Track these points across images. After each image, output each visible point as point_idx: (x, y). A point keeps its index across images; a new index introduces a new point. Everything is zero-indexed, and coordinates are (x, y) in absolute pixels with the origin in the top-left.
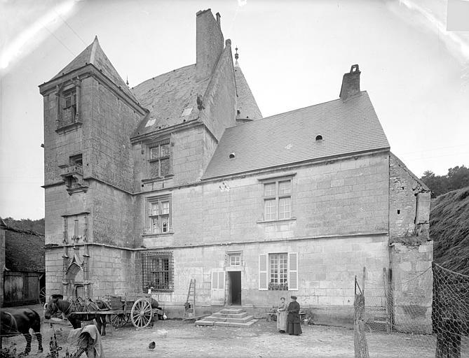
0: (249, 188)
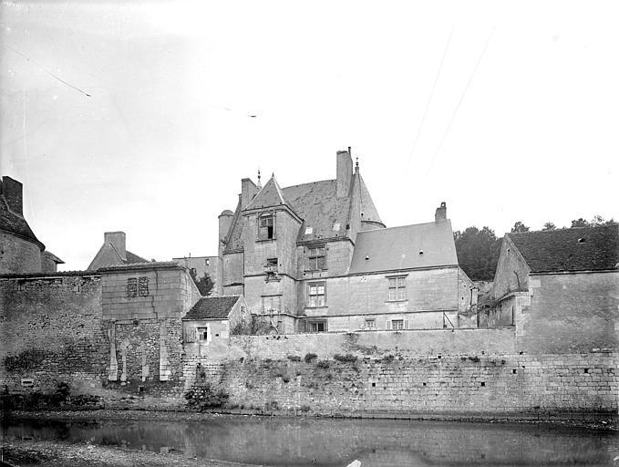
0: (380, 281)
